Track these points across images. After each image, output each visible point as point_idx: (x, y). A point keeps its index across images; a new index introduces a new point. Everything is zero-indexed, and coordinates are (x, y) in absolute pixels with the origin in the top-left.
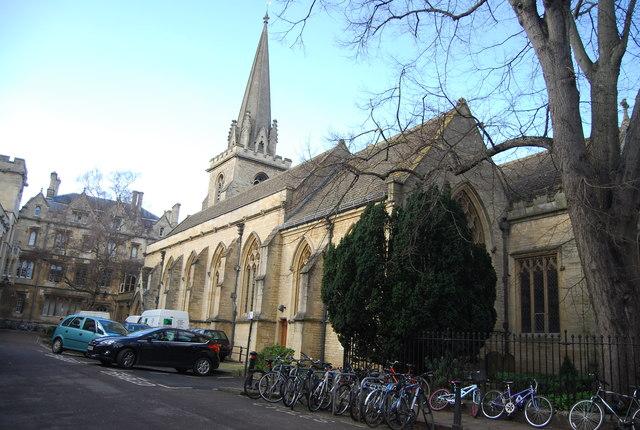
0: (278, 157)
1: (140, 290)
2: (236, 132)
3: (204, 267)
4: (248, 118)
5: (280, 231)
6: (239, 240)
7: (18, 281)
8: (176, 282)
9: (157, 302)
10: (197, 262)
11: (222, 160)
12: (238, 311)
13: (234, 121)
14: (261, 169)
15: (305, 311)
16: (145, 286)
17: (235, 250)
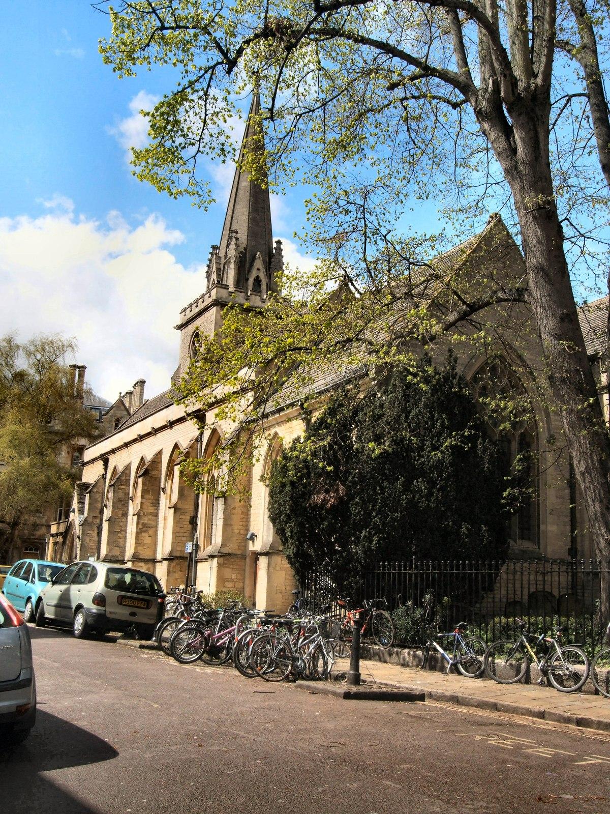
1: (76, 518)
4: (233, 242)
8: (122, 503)
10: (146, 473)
11: (196, 310)
13: (215, 248)
16: (81, 511)
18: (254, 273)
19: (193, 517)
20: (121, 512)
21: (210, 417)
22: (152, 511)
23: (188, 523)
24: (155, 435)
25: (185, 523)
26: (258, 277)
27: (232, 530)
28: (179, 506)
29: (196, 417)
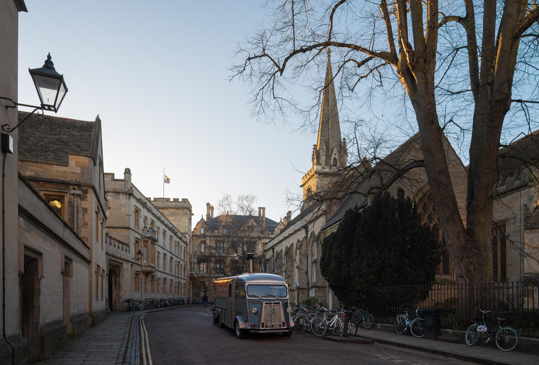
2: (317, 155)
5: (324, 230)
7: (200, 275)
13: (315, 146)
18: (333, 156)
20: (280, 270)
21: (310, 227)
24: (296, 233)
26: (335, 158)
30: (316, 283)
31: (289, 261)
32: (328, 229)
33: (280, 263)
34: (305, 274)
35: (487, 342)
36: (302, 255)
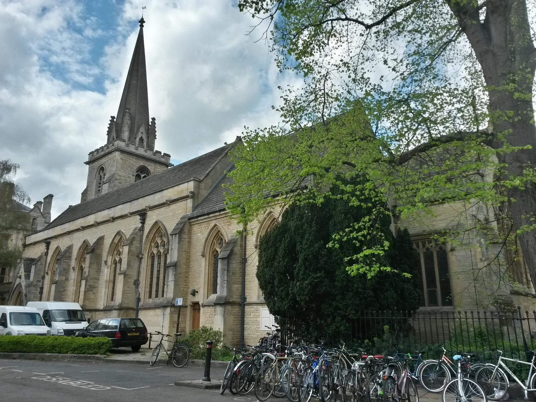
0: (158, 152)
3: (99, 257)
4: (127, 115)
5: (190, 219)
6: (142, 229)
9: (41, 293)
10: (93, 251)
11: (102, 153)
12: (142, 297)
13: (113, 118)
14: (142, 163)
15: (225, 294)
16: (28, 277)
17: (138, 238)
18: (140, 135)
19: (136, 280)
22: (96, 276)
23: (133, 284)
25: (130, 284)
26: (142, 137)
27: (180, 288)
28: (127, 273)
29: (140, 215)
30: (173, 300)
31: (94, 263)
32: (199, 219)
33: (65, 266)
34: (134, 284)
35: (528, 396)
36: (132, 255)
